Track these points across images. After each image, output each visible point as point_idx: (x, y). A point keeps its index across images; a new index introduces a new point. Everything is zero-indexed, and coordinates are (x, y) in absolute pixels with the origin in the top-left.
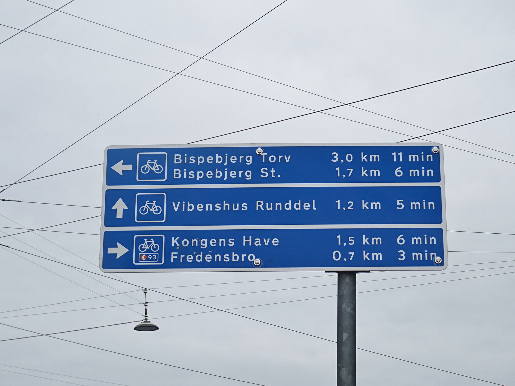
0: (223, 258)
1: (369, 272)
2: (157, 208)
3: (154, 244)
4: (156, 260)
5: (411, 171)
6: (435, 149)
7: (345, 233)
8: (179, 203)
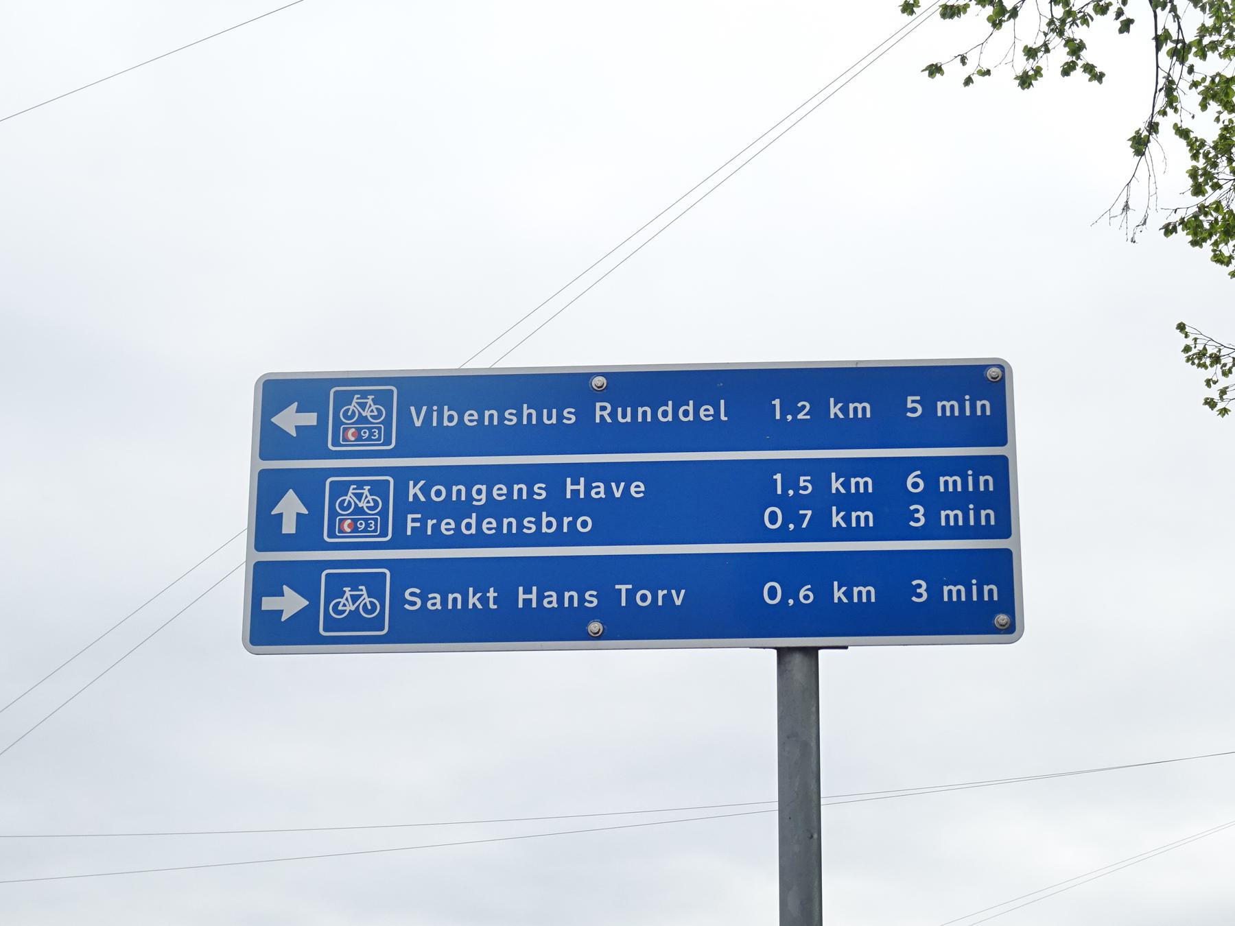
0: (520, 526)
1: (846, 648)
2: (377, 409)
3: (367, 600)
4: (375, 530)
5: (943, 514)
6: (993, 372)
7: (792, 470)
8: (424, 408)
